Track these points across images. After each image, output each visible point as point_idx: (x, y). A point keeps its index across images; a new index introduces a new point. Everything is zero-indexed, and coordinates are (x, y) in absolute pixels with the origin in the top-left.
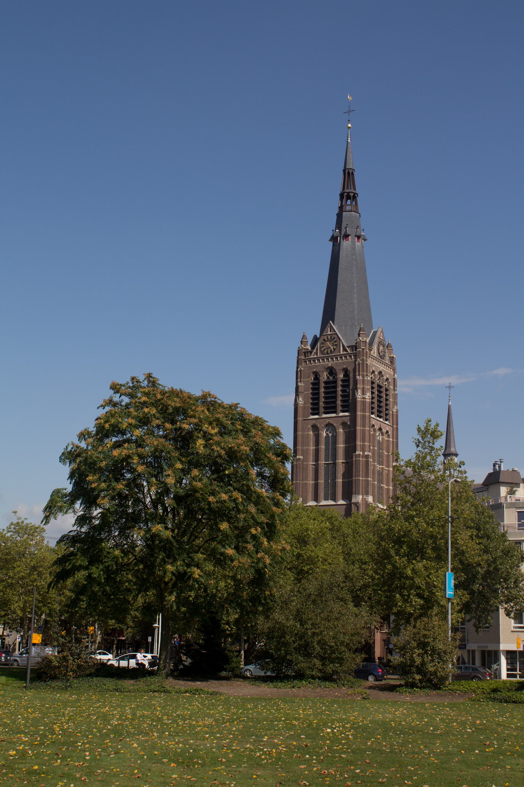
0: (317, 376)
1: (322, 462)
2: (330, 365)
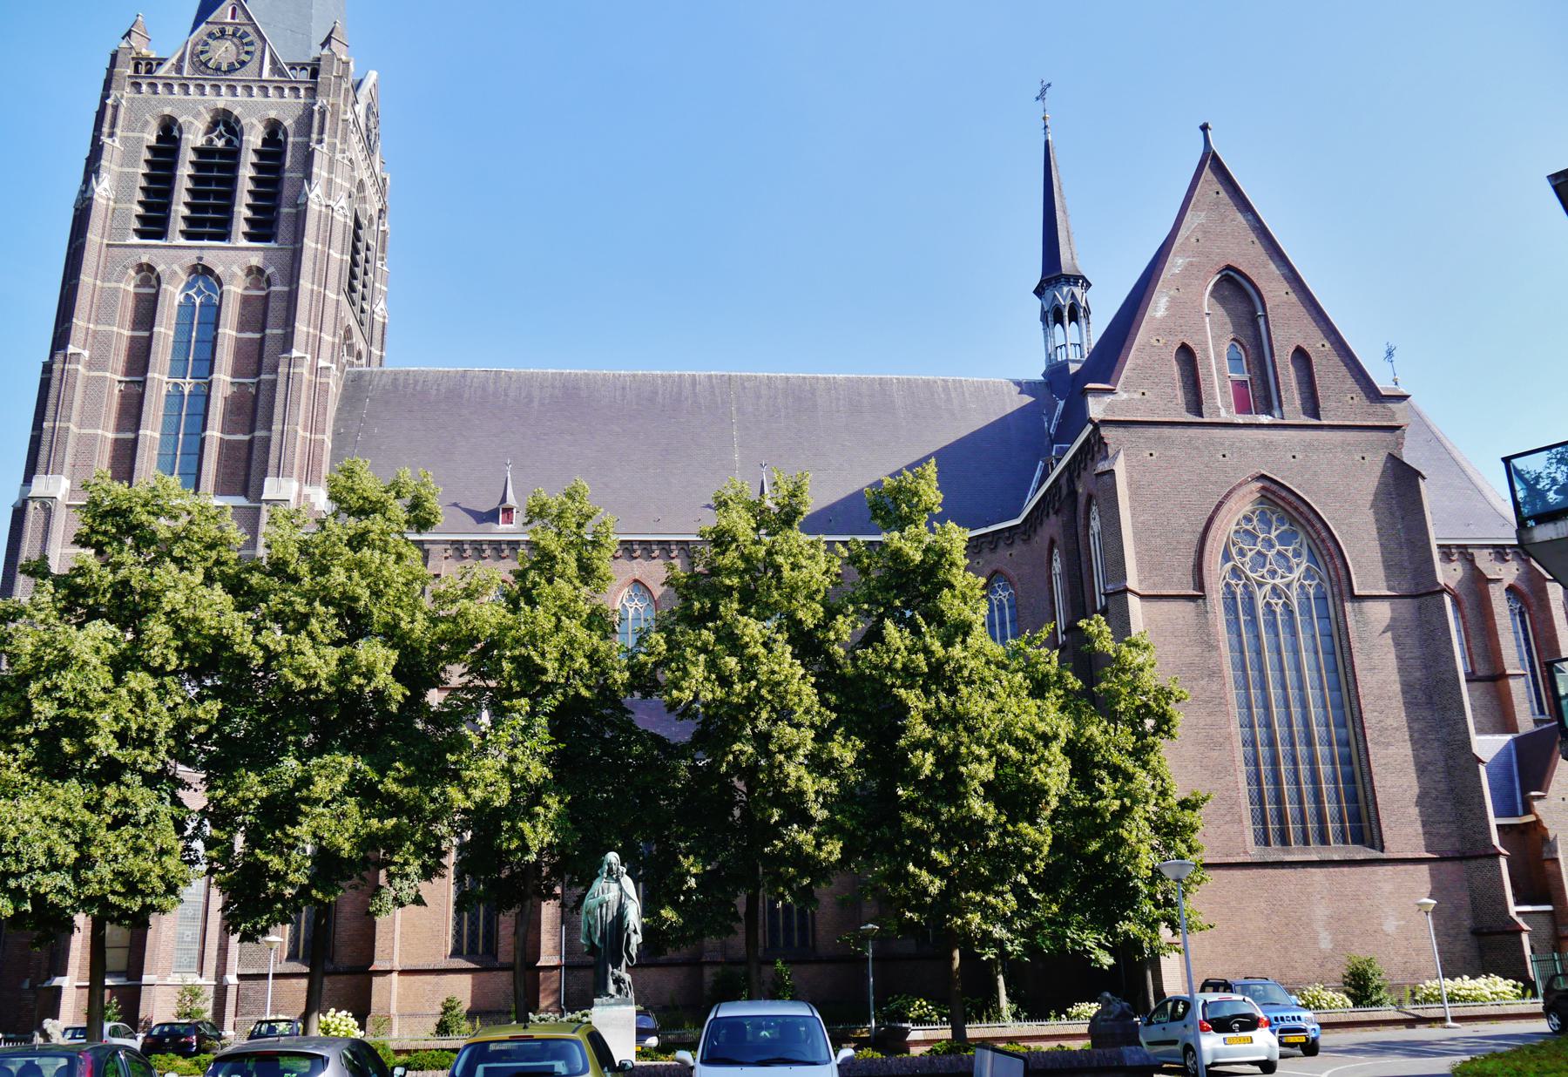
0: (169, 134)
1: (160, 378)
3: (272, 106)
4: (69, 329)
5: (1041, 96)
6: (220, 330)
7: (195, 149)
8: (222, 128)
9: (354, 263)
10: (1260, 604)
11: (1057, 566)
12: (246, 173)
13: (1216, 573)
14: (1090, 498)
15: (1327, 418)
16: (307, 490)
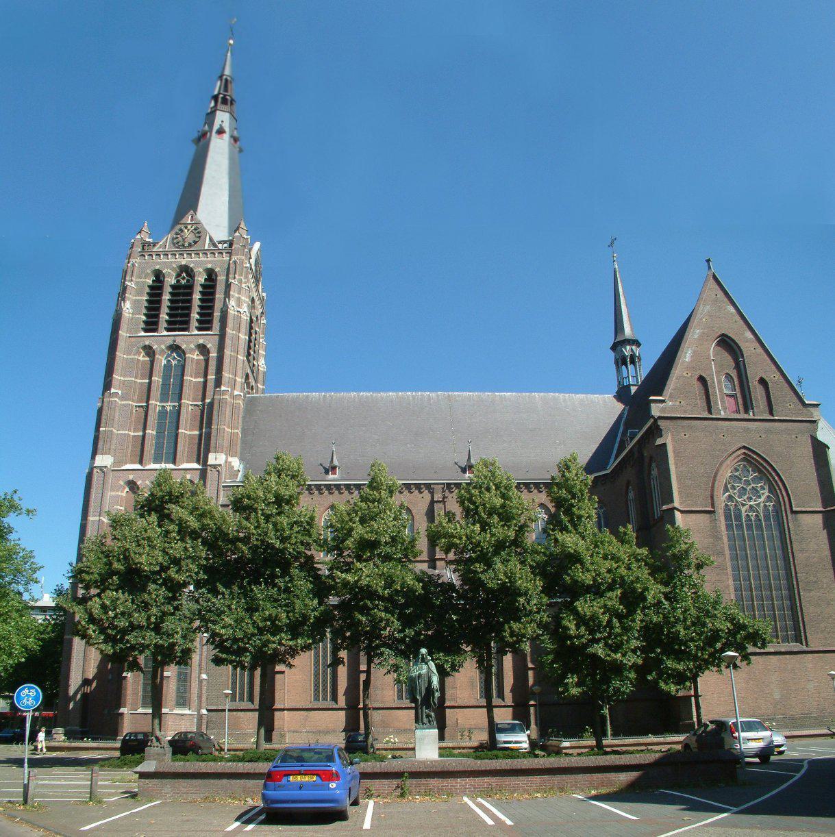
0: (159, 276)
2: (183, 263)
3: (210, 262)
4: (111, 381)
5: (611, 245)
6: (185, 378)
7: (171, 286)
8: (184, 274)
9: (250, 341)
10: (744, 515)
11: (631, 495)
12: (197, 296)
13: (721, 499)
14: (651, 458)
15: (777, 416)
16: (230, 459)
